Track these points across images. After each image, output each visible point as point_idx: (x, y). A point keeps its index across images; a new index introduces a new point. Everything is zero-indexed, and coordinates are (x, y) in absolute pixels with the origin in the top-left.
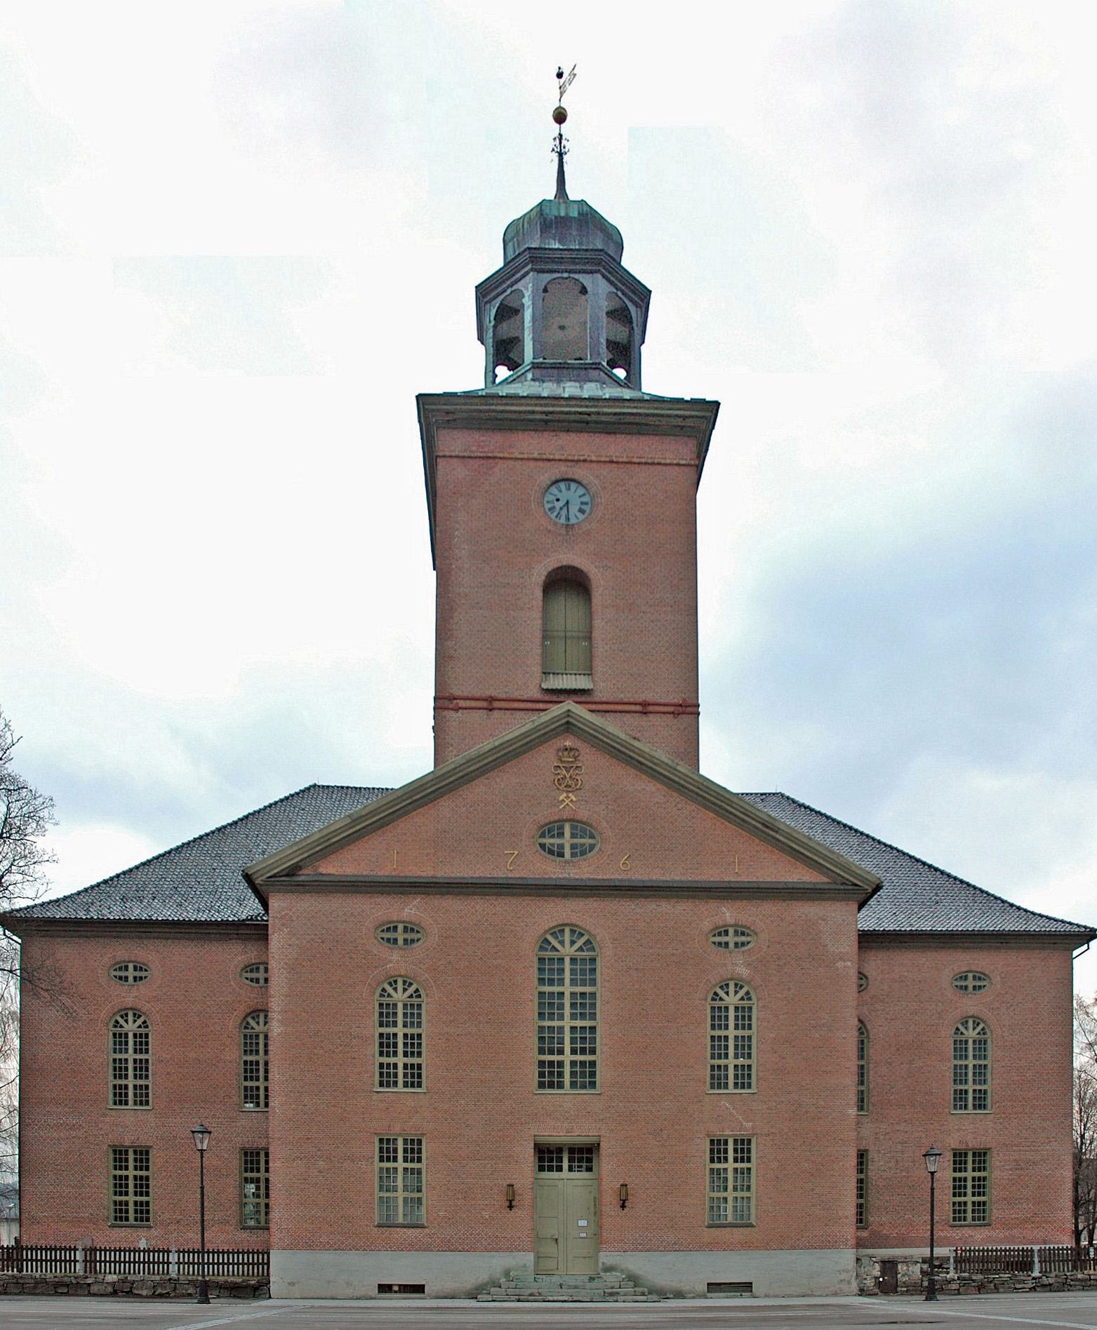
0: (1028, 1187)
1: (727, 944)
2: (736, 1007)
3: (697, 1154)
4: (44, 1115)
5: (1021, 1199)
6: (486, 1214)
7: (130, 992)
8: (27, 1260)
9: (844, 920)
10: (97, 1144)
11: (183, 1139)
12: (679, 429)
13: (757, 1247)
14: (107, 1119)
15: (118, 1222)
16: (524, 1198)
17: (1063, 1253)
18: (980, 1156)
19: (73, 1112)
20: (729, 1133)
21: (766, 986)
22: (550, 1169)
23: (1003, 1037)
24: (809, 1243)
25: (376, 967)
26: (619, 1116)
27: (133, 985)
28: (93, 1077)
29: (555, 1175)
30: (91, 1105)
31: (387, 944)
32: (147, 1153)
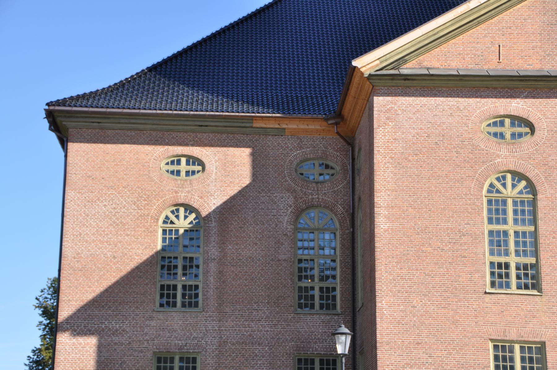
2: (163, 230)
4: (85, 319)
7: (182, 187)
10: (141, 351)
11: (233, 344)
14: (153, 323)
18: (190, 289)
19: (116, 315)
25: (483, 162)
27: (186, 180)
28: (140, 277)
30: (137, 308)
31: (495, 139)
32: (194, 360)
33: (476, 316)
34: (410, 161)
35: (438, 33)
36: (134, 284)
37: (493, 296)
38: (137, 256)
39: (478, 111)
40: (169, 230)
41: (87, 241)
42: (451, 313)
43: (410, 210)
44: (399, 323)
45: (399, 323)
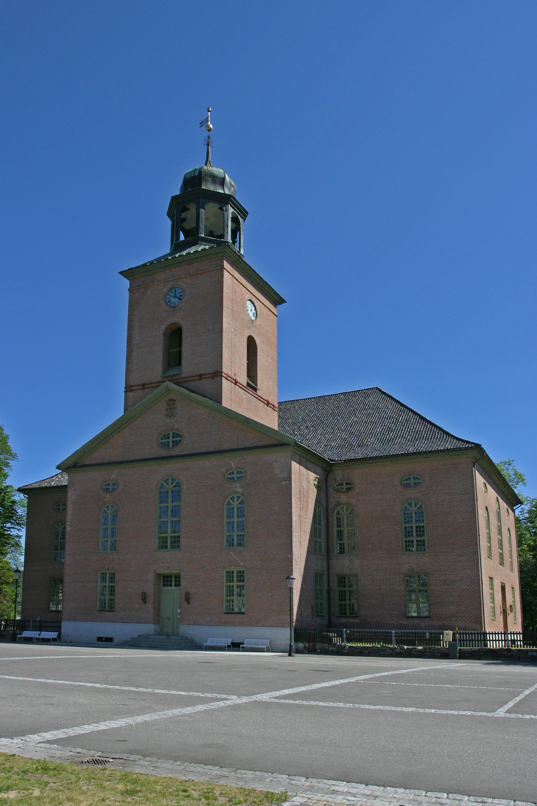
0: (452, 595)
1: (233, 478)
3: (219, 578)
5: (448, 603)
6: (136, 606)
8: (490, 640)
9: (285, 461)
12: (215, 255)
13: (246, 625)
15: (352, 615)
16: (151, 598)
17: (421, 636)
20: (235, 569)
21: (249, 496)
22: (167, 585)
23: (432, 510)
24: (270, 623)
26: (188, 560)
29: (169, 588)
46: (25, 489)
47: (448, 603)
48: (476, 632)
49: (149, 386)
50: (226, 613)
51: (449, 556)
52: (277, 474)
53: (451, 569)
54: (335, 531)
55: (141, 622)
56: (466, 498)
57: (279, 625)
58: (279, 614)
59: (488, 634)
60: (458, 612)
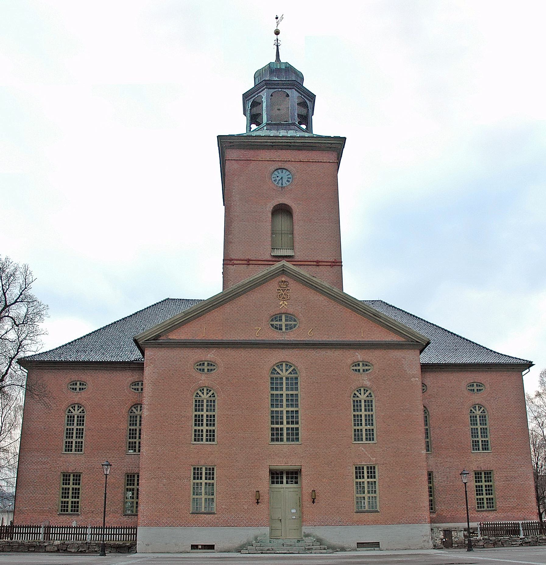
1: (359, 370)
3: (349, 474)
8: (52, 534)
10: (56, 472)
20: (364, 463)
24: (407, 520)
27: (79, 392)
28: (56, 438)
29: (280, 485)
30: (54, 452)
31: (200, 372)
33: (186, 455)
34: (160, 382)
35: (174, 323)
36: (53, 441)
37: (195, 445)
38: (55, 428)
39: (193, 359)
40: (199, 400)
41: (33, 421)
42: (175, 453)
43: (159, 406)
44: (150, 458)
45: (150, 458)
46: (31, 362)
47: (511, 496)
48: (493, 523)
49: (254, 262)
50: (192, 513)
51: (509, 456)
52: (406, 370)
53: (511, 467)
54: (137, 431)
55: (253, 525)
56: (519, 405)
57: (415, 522)
58: (415, 511)
59: (51, 527)
60: (518, 504)
